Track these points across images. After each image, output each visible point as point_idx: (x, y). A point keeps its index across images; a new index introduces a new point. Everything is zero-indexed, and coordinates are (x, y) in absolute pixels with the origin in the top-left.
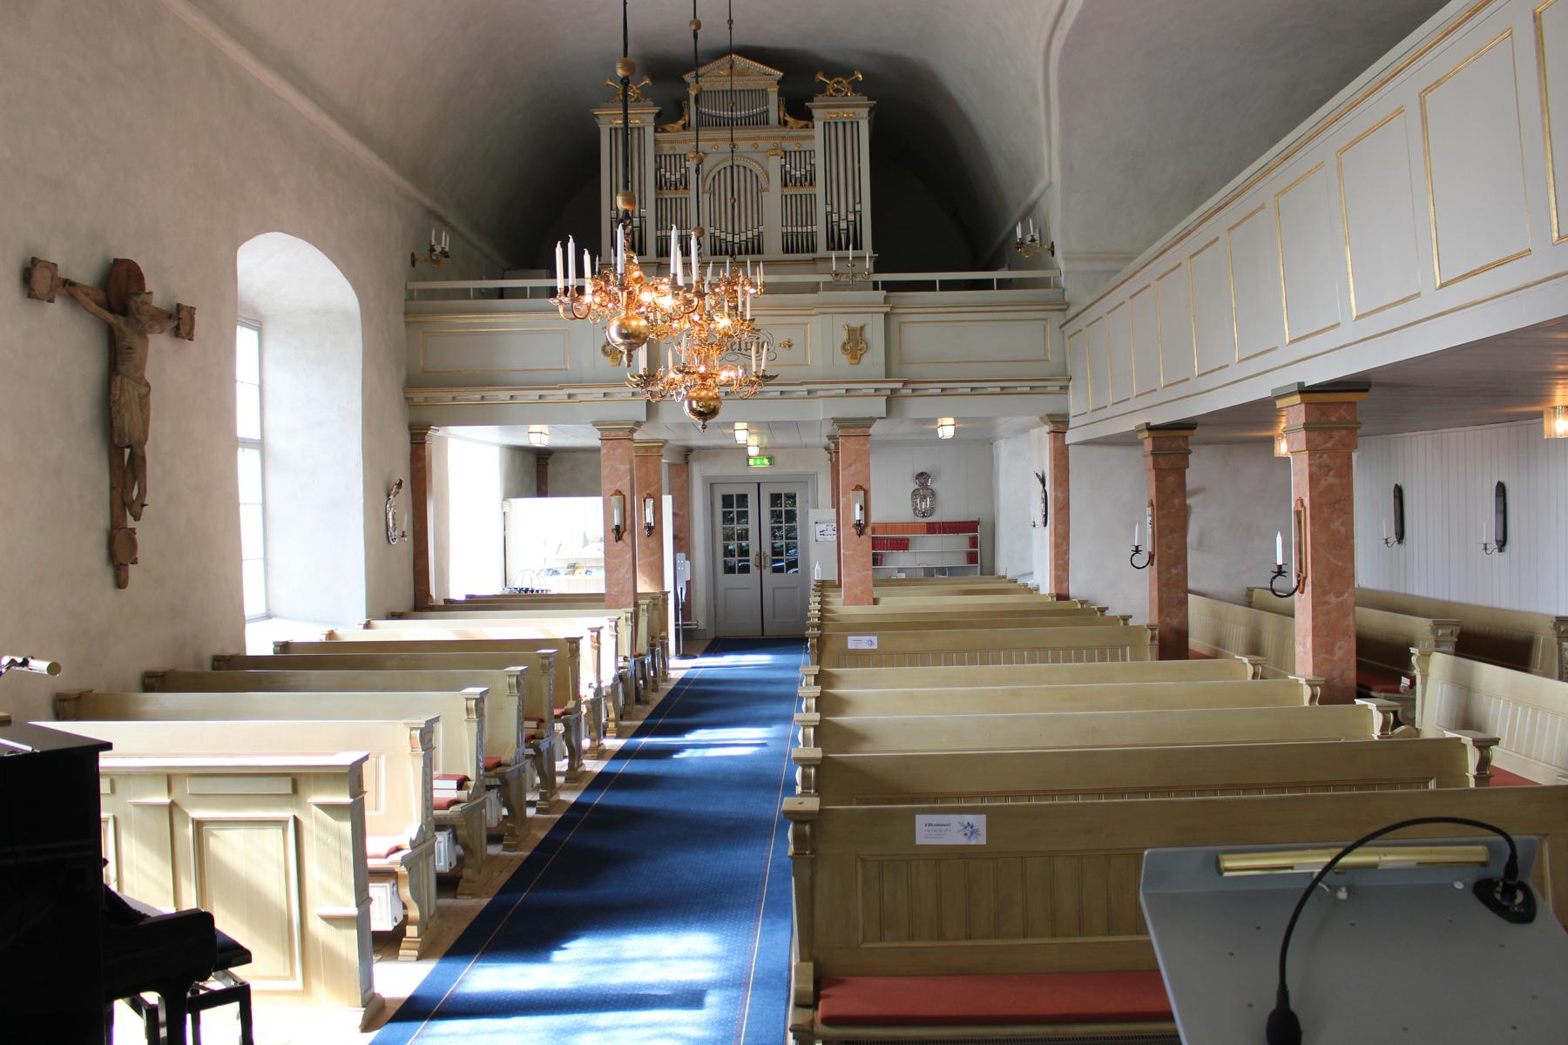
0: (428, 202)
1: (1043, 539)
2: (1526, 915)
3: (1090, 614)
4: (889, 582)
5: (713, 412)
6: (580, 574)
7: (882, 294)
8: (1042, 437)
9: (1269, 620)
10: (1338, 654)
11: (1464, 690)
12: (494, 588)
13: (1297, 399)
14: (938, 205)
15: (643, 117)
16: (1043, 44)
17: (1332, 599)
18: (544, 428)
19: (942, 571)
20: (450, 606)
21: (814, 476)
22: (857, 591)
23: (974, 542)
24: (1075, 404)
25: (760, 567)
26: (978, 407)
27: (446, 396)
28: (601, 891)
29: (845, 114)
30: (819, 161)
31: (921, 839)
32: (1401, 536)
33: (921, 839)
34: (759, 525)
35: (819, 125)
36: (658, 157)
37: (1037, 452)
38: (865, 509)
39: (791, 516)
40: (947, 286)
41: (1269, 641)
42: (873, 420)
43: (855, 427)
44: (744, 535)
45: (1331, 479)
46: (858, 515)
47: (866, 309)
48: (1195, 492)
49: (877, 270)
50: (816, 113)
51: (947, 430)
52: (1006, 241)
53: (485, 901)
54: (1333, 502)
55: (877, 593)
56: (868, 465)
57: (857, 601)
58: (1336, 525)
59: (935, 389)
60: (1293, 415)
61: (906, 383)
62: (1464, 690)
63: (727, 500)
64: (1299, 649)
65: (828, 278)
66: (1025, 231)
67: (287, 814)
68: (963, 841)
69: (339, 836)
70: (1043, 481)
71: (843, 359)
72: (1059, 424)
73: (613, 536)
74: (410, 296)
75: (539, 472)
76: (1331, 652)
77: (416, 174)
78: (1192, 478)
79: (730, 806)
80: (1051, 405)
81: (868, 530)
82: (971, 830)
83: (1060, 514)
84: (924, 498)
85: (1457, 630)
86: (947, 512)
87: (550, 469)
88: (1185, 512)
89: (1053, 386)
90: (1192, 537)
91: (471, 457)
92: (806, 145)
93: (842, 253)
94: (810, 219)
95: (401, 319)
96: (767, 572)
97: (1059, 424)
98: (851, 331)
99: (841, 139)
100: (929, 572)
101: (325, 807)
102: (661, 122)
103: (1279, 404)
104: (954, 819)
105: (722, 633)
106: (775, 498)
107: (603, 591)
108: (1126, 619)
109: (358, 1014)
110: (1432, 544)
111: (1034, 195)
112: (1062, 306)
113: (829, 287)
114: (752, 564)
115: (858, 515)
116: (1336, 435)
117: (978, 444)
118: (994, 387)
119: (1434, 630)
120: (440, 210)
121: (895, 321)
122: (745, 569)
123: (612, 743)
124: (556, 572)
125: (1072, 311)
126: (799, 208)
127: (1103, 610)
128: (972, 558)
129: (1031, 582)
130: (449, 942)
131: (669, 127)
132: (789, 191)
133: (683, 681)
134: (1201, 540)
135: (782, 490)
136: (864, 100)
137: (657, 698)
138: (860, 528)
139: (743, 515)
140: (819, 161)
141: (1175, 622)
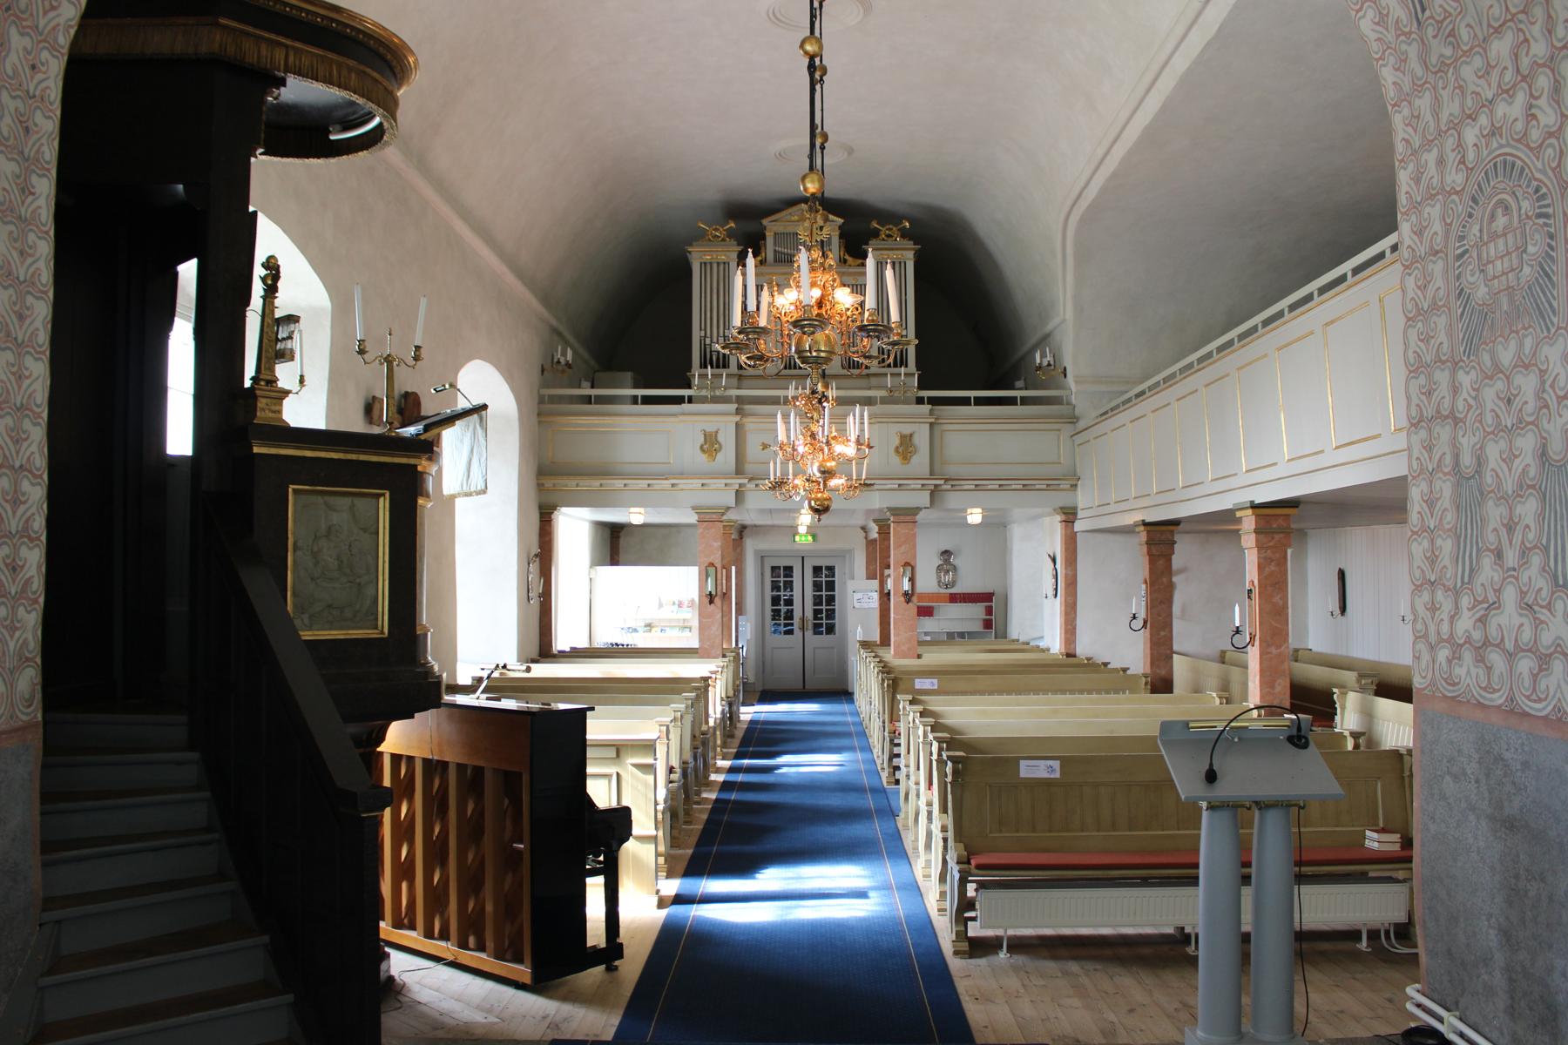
0: (554, 322)
1: (1053, 611)
2: (1305, 746)
5: (826, 509)
6: (656, 632)
7: (926, 408)
8: (1055, 524)
9: (1235, 671)
10: (1278, 689)
11: (1368, 714)
12: (582, 643)
13: (1250, 512)
14: (965, 331)
16: (1062, 217)
17: (1273, 650)
18: (642, 510)
19: (962, 635)
20: (576, 654)
21: (851, 551)
22: (904, 648)
23: (989, 611)
24: (1083, 499)
25: (803, 629)
26: (1000, 500)
27: (571, 484)
28: (770, 844)
31: (1023, 774)
32: (1343, 609)
33: (1023, 774)
35: (870, 262)
37: (1052, 537)
38: (912, 580)
39: (831, 586)
40: (980, 401)
41: (1235, 689)
42: (919, 509)
43: (907, 515)
44: (789, 602)
45: (1273, 568)
46: (906, 586)
47: (916, 421)
48: (1181, 571)
49: (921, 387)
51: (975, 517)
52: (1023, 358)
53: (690, 851)
54: (1274, 586)
55: (920, 650)
56: (914, 546)
58: (1277, 599)
59: (970, 485)
60: (1249, 522)
61: (947, 480)
62: (1368, 714)
64: (1251, 684)
65: (883, 393)
66: (1043, 356)
67: (612, 770)
68: (1046, 775)
69: (646, 784)
70: (1054, 560)
71: (896, 460)
72: (1069, 515)
73: (707, 600)
74: (541, 400)
75: (615, 544)
76: (1273, 687)
77: (546, 300)
78: (1177, 561)
79: (834, 801)
80: (1063, 499)
81: (915, 599)
84: (947, 572)
85: (1376, 680)
86: (965, 585)
87: (622, 541)
88: (1171, 587)
89: (1065, 485)
90: (1176, 609)
91: (574, 529)
93: (896, 370)
95: (534, 419)
96: (809, 633)
97: (1069, 515)
100: (951, 635)
101: (636, 766)
103: (1238, 514)
104: (1042, 763)
105: (769, 686)
106: (817, 570)
107: (696, 645)
108: (1125, 670)
109: (655, 900)
110: (1365, 614)
111: (1049, 327)
112: (1073, 419)
113: (884, 401)
114: (796, 627)
115: (906, 586)
116: (1277, 537)
117: (996, 526)
118: (1017, 485)
119: (1359, 681)
120: (562, 328)
121: (937, 429)
122: (790, 632)
123: (727, 764)
124: (635, 630)
125: (1081, 425)
127: (1105, 664)
128: (988, 624)
129: (1042, 644)
130: (682, 866)
133: (752, 722)
134: (1183, 611)
135: (823, 563)
136: (910, 244)
137: (740, 734)
138: (908, 597)
139: (789, 585)
141: (1163, 672)
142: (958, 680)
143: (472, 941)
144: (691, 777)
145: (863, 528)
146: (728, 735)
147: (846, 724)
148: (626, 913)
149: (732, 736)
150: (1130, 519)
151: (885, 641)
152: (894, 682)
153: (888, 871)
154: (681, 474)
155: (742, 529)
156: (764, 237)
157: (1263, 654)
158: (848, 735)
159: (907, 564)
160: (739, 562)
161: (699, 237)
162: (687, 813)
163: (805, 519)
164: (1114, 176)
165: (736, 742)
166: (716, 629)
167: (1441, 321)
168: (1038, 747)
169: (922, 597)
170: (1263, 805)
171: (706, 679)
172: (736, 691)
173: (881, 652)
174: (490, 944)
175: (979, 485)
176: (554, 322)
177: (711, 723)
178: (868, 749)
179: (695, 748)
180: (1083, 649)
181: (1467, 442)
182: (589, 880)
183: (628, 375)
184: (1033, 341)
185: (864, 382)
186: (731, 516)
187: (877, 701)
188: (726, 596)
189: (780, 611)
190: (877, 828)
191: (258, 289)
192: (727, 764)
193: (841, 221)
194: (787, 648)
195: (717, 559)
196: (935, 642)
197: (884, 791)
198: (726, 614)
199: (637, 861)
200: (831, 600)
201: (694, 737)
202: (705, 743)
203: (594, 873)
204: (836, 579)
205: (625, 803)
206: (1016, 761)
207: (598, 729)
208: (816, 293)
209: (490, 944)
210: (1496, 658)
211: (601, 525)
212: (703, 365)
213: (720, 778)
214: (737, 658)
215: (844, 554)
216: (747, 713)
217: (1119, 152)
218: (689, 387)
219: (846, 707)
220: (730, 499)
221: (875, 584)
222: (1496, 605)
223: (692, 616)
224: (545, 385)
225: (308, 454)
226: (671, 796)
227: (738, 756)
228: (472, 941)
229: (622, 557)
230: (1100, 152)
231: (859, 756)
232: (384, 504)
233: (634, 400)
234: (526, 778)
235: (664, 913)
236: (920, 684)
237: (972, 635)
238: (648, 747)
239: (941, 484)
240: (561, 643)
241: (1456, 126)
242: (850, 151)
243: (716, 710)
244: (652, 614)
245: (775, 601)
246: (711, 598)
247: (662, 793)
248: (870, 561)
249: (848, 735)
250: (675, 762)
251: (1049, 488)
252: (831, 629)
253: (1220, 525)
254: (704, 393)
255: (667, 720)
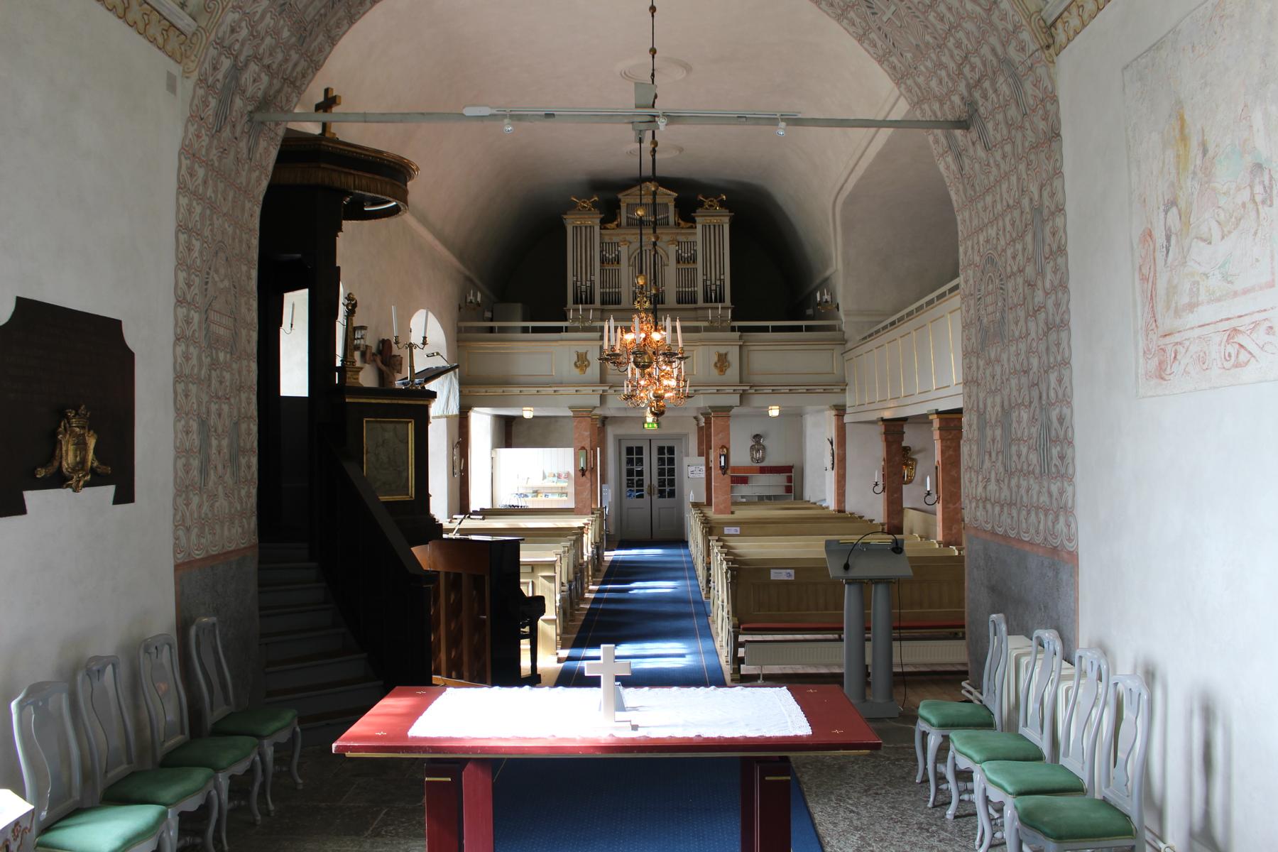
0: (468, 273)
1: (831, 477)
3: (855, 519)
4: (735, 503)
5: (662, 413)
6: (541, 497)
7: (737, 334)
8: (830, 415)
12: (488, 506)
15: (594, 221)
17: (951, 506)
19: (769, 498)
21: (686, 435)
22: (722, 507)
23: (789, 479)
24: (850, 399)
25: (650, 494)
26: (795, 401)
27: (482, 391)
29: (714, 220)
30: (699, 248)
34: (650, 467)
35: (699, 227)
36: (601, 243)
39: (671, 461)
40: (775, 329)
42: (731, 407)
44: (640, 473)
49: (733, 319)
50: (698, 219)
51: (774, 412)
55: (733, 508)
57: (721, 512)
58: (953, 473)
59: (768, 390)
63: (630, 451)
71: (715, 372)
74: (459, 330)
75: (510, 433)
77: (461, 256)
79: (669, 608)
80: (836, 399)
81: (729, 472)
82: (789, 575)
83: (840, 463)
84: (758, 451)
86: (773, 460)
89: (837, 389)
91: (481, 422)
92: (691, 238)
94: (693, 283)
96: (655, 497)
97: (840, 411)
98: (720, 355)
99: (711, 238)
100: (761, 498)
102: (604, 222)
104: (783, 571)
106: (661, 450)
108: (871, 521)
109: (555, 659)
111: (828, 273)
112: (843, 341)
113: (707, 329)
114: (645, 493)
117: (793, 418)
121: (745, 349)
122: (641, 496)
123: (596, 588)
124: (526, 496)
125: (849, 345)
126: (687, 277)
127: (861, 517)
128: (788, 489)
131: (608, 226)
132: (680, 266)
135: (666, 444)
136: (726, 212)
138: (724, 469)
139: (640, 461)
140: (699, 248)
141: (895, 522)
142: (752, 528)
143: (454, 674)
144: (574, 594)
145: (695, 418)
146: (597, 569)
147: (681, 562)
148: (540, 665)
149: (599, 571)
150: (874, 416)
151: (709, 503)
152: (710, 529)
153: (700, 644)
154: (561, 384)
155: (604, 420)
156: (619, 207)
157: (944, 508)
158: (682, 569)
159: (723, 447)
160: (602, 443)
161: (572, 207)
162: (572, 614)
163: (650, 418)
164: (862, 178)
165: (602, 574)
166: (586, 494)
167: (973, 331)
168: (782, 563)
169: (735, 469)
170: (877, 581)
171: (581, 528)
172: (601, 538)
173: (706, 510)
174: (466, 674)
175: (775, 390)
176: (468, 273)
177: (585, 558)
178: (696, 578)
179: (575, 573)
180: (850, 507)
181: (982, 395)
182: (522, 641)
183: (518, 308)
184: (818, 281)
185: (692, 314)
186: (597, 412)
187: (700, 545)
188: (593, 470)
189: (633, 480)
190: (695, 623)
191: (342, 310)
192: (596, 588)
193: (676, 195)
194: (640, 507)
195: (587, 444)
196: (749, 502)
197: (703, 602)
198: (593, 484)
199: (544, 634)
200: (672, 472)
201: (575, 567)
202: (582, 571)
203: (525, 637)
204: (676, 456)
205: (538, 593)
206: (768, 570)
207: (527, 555)
208: (643, 335)
209: (466, 674)
210: (989, 506)
211: (498, 418)
212: (576, 302)
213: (592, 596)
214: (601, 515)
215: (681, 437)
216: (609, 556)
217: (864, 164)
218: (566, 320)
219: (682, 551)
220: (597, 402)
221: (703, 459)
222: (989, 480)
223: (569, 486)
224: (461, 319)
225: (373, 401)
226: (562, 599)
227: (604, 583)
228: (454, 674)
229: (514, 440)
230: (852, 164)
231: (688, 582)
232: (411, 427)
233: (525, 330)
234: (487, 578)
235: (561, 665)
236: (727, 530)
237: (776, 498)
238: (551, 565)
239: (748, 389)
240: (474, 505)
241: (1002, 215)
242: (681, 150)
243: (588, 551)
244: (537, 482)
245: (630, 473)
246: (583, 472)
247: (558, 597)
248: (700, 443)
249: (682, 569)
250: (564, 580)
251: (825, 391)
252: (672, 494)
253: (923, 420)
254: (576, 324)
255: (560, 551)
